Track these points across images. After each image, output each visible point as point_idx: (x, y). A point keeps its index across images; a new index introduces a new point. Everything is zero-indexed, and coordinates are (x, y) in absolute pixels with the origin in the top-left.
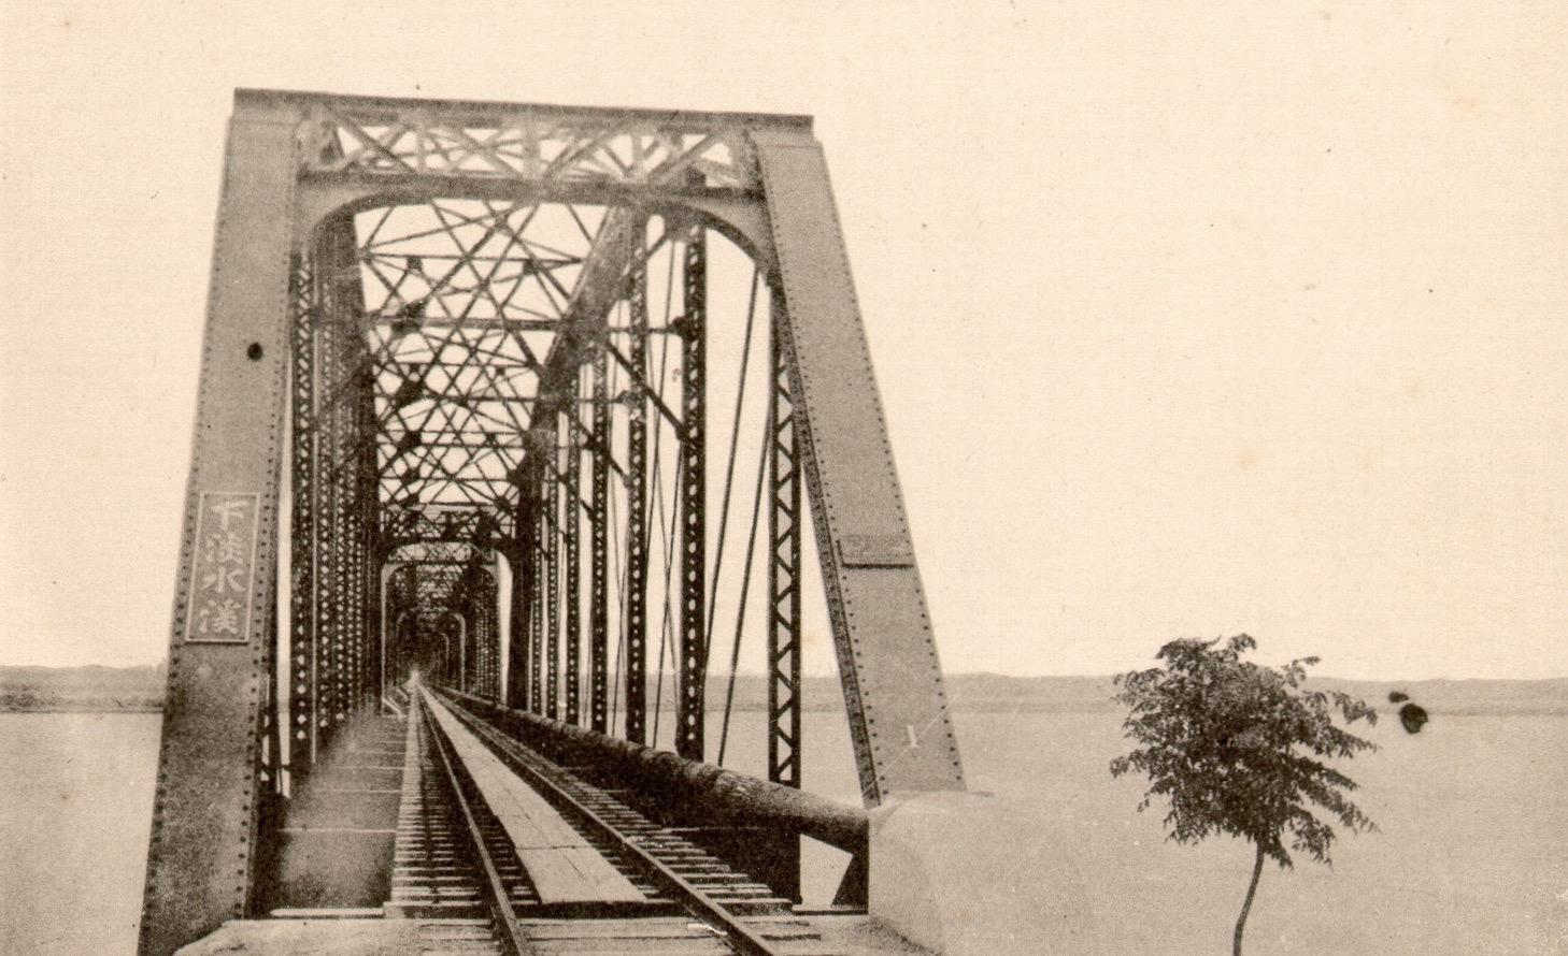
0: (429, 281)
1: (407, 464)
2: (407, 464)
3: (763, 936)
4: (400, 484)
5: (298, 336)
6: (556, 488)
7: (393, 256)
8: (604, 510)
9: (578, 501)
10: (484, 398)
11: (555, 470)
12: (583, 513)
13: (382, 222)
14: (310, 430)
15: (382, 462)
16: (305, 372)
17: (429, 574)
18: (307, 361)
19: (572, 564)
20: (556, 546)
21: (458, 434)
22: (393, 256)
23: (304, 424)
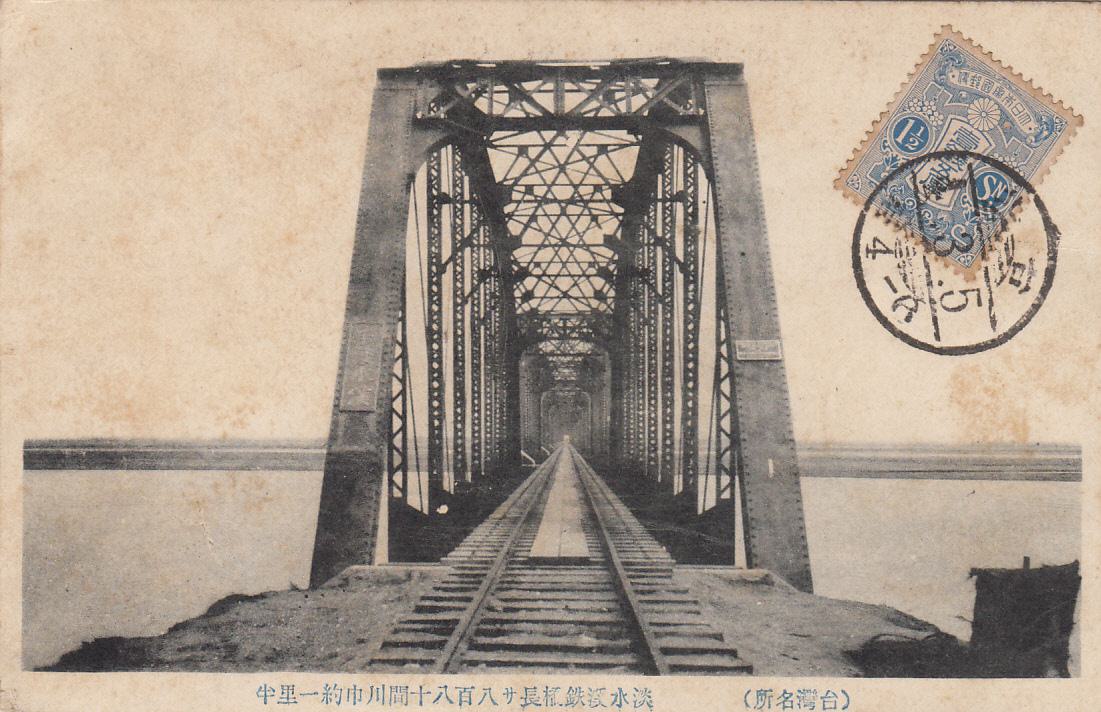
0: (530, 159)
1: (522, 234)
2: (522, 234)
3: (465, 609)
4: (494, 113)
5: (455, 223)
6: (655, 251)
7: (508, 146)
8: (695, 263)
9: (674, 258)
10: (580, 276)
11: (652, 232)
12: (677, 267)
13: (509, 171)
14: (462, 305)
15: (517, 305)
16: (435, 178)
17: (563, 363)
18: (436, 171)
19: (691, 327)
20: (695, 184)
21: (563, 213)
22: (508, 146)
23: (459, 301)
